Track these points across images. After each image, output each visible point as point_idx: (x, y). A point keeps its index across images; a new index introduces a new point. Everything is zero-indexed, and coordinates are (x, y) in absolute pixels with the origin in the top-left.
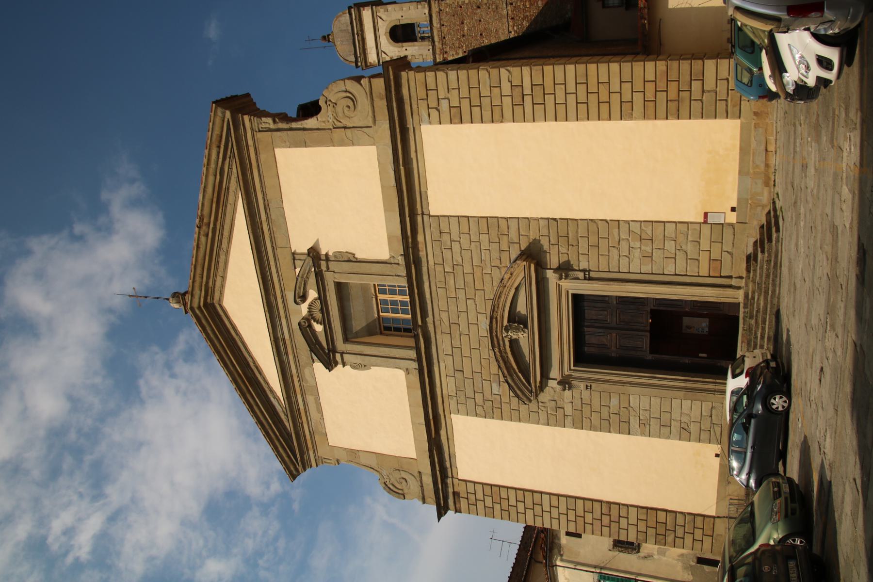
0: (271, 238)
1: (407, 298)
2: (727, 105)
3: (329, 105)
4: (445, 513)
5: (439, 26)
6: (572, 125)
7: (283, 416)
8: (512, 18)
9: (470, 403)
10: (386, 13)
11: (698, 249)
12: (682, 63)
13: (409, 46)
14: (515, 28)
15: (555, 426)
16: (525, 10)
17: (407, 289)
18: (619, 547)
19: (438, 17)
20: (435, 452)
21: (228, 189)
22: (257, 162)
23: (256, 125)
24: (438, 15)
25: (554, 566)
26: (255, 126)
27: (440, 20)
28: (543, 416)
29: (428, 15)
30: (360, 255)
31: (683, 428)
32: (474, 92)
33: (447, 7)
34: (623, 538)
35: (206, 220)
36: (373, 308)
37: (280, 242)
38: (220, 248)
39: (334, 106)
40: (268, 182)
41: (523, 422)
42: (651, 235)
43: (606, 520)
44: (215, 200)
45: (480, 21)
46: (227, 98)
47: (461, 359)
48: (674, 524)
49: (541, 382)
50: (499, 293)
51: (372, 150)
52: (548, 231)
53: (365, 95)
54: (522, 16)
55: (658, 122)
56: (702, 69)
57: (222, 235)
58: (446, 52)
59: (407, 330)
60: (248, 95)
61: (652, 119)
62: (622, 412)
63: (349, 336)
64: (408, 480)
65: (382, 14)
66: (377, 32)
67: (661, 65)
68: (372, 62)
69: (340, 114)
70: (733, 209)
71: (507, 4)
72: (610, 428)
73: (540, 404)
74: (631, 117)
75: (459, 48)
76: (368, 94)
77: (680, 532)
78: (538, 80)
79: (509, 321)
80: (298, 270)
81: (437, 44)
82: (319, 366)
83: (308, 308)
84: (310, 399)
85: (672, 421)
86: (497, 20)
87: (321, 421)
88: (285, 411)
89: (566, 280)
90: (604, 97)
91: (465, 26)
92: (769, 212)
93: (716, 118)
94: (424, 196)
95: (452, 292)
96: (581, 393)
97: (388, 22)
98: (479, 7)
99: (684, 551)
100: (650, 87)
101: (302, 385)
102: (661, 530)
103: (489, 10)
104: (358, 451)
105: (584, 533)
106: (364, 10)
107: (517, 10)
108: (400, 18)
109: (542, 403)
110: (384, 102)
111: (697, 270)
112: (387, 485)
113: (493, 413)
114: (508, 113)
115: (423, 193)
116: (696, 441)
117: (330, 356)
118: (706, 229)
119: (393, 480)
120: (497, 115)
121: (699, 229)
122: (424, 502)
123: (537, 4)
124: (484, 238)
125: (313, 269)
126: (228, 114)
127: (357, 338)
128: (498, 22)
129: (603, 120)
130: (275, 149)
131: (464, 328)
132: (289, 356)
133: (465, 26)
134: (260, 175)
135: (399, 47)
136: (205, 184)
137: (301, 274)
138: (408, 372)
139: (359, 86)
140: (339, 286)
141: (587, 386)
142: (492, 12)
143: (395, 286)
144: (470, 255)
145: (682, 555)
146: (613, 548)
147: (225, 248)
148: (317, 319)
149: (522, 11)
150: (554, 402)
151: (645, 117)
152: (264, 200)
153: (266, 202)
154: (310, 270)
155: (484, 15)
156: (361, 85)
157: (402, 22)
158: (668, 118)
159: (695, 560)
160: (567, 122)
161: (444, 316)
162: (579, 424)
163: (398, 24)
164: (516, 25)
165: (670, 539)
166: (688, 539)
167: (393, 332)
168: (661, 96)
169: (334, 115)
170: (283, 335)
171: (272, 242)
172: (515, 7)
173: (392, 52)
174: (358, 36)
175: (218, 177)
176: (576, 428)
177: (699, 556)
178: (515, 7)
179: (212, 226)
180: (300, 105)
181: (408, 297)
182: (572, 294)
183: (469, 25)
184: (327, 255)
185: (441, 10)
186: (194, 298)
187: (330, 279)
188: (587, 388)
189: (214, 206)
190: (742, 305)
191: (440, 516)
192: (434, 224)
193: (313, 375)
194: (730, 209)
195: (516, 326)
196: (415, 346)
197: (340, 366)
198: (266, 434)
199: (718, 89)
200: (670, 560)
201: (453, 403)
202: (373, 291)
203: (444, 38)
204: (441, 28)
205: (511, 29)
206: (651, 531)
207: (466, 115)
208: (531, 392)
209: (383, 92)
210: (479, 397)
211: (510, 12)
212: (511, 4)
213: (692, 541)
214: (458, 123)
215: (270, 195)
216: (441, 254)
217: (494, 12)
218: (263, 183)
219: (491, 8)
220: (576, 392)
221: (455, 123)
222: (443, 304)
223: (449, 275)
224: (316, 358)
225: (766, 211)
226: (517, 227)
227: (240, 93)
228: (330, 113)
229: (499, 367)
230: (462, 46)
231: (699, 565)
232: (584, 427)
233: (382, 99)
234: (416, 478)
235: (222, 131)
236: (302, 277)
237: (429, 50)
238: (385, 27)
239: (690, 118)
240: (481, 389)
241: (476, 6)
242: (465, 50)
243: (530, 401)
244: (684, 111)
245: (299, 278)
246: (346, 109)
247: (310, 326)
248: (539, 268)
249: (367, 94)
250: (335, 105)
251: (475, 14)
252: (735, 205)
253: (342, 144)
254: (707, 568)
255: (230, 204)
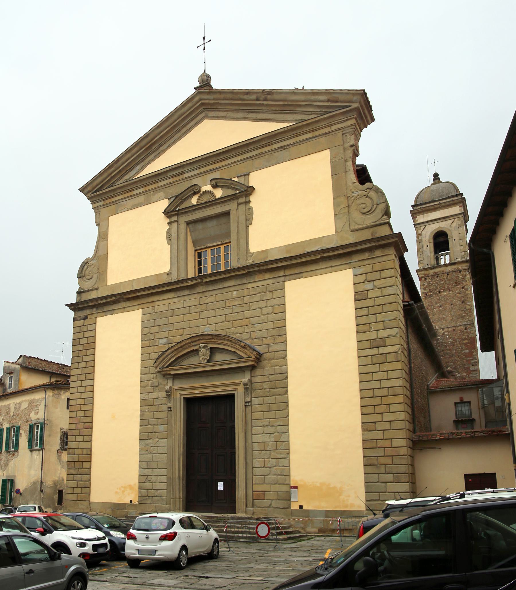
0: (259, 154)
1: (223, 269)
2: (375, 500)
3: (366, 191)
4: (71, 309)
5: (447, 271)
6: (357, 386)
7: (126, 178)
8: (454, 330)
9: (151, 323)
10: (457, 226)
11: (271, 483)
12: (406, 466)
13: (430, 248)
14: (446, 333)
15: (141, 387)
16: (461, 340)
17: (230, 268)
18: (64, 436)
19: (454, 270)
20: (113, 299)
21: (295, 113)
22: (318, 136)
23: (348, 131)
24: (456, 270)
25: (45, 390)
26: (347, 130)
27: (452, 272)
28: (146, 377)
29: (456, 261)
30: (251, 228)
31: (147, 477)
32: (379, 309)
33: (462, 277)
34: (70, 438)
35: (269, 97)
36: (213, 242)
37: (257, 162)
38: (248, 112)
39: (365, 195)
40: (302, 147)
41: (141, 363)
42: (279, 449)
43: (80, 426)
44: (286, 103)
45: (452, 305)
46: (369, 102)
47: (182, 313)
48: (82, 474)
49: (170, 375)
50: (230, 339)
51: (331, 231)
52: (278, 373)
53: (375, 221)
54: (456, 338)
55: (361, 450)
56: (402, 481)
57: (259, 113)
58: (426, 279)
59: (200, 271)
60: (373, 120)
61: (363, 446)
62: (155, 434)
63: (191, 226)
64: (92, 280)
65: (457, 223)
66: (441, 220)
67: (404, 451)
68: (417, 219)
69: (358, 202)
70: (301, 507)
71: (465, 325)
72: (143, 426)
73: (155, 375)
74: (364, 430)
75: (430, 290)
76: (375, 223)
77: (78, 478)
78: (390, 358)
79: (211, 348)
80: (236, 179)
81: (432, 271)
82: (165, 204)
83: (208, 191)
84: (141, 198)
85: (152, 469)
86: (453, 318)
87: (126, 209)
88: (130, 179)
89: (243, 389)
90: (378, 409)
91: (447, 293)
92: (300, 532)
93: (366, 492)
94: (299, 275)
95: (229, 303)
96: (166, 404)
97: (450, 228)
98: (463, 302)
99: (65, 481)
100: (387, 443)
101: (151, 191)
102: (77, 465)
103: (460, 311)
104: (108, 240)
105: (70, 411)
106: (460, 207)
107: (461, 333)
108: (454, 239)
109: (156, 376)
110: (370, 237)
111: (257, 482)
112: (86, 264)
113: (146, 341)
114: (364, 336)
115: (301, 275)
116: (139, 486)
117: (175, 212)
118: (284, 488)
119: (90, 268)
120: (361, 328)
121: (286, 483)
122: (77, 293)
123: (466, 349)
124: (271, 325)
125: (238, 192)
126: (355, 105)
127: (190, 232)
128: (451, 319)
129: (361, 409)
130: (329, 150)
131: (205, 314)
132: (171, 179)
133: (447, 293)
134: (307, 139)
135: (429, 240)
136: (298, 92)
137: (233, 182)
138: (169, 274)
139: (381, 216)
140: (227, 214)
141: (171, 408)
142: (459, 313)
143: (230, 259)
144: (258, 316)
145: (63, 480)
146: (63, 432)
147: (249, 117)
148: (202, 197)
149: (460, 337)
150: (157, 385)
151: (364, 441)
152: (288, 145)
153: (287, 147)
154: (237, 189)
155: (457, 307)
156: (383, 216)
157: (449, 240)
158: (365, 458)
159: (61, 489)
160: (359, 382)
161: (211, 299)
162: (144, 403)
163: (449, 237)
164: (449, 333)
165: (72, 471)
166: (72, 484)
167: (197, 260)
168: (381, 452)
169: (358, 197)
170: (186, 172)
171: (257, 155)
172: (463, 332)
173: (425, 235)
174: (438, 204)
175: (304, 103)
176: (141, 402)
177: (64, 492)
178: (463, 332)
179: (265, 103)
180: (366, 166)
181: (224, 270)
182: (234, 393)
183: (448, 296)
184: (250, 202)
185: (460, 272)
186: (208, 94)
187: (231, 206)
188: (169, 408)
189: (281, 103)
190: (233, 515)
191: (69, 306)
192: (278, 286)
193: (159, 200)
194: (301, 505)
195: (208, 354)
196: (188, 278)
197: (168, 221)
198: (111, 166)
199: (387, 494)
200: (59, 472)
201: (150, 310)
202: (226, 241)
203: (437, 277)
204: (445, 273)
205: (446, 329)
206: (76, 458)
207: (361, 304)
208: (163, 368)
209: (377, 235)
210: (155, 329)
211: (459, 328)
212: (466, 329)
213: (72, 486)
214: (355, 298)
215: (293, 149)
216: (257, 293)
217: (459, 315)
218: (303, 142)
219: (462, 312)
220: (164, 401)
221: (355, 296)
222: (220, 297)
223: (241, 300)
224: (172, 200)
225: (301, 530)
226: (279, 350)
227: (374, 112)
228: (360, 192)
229: (178, 343)
230: (431, 292)
231: (58, 491)
232: (142, 407)
233: (372, 235)
234: (93, 286)
235: (341, 102)
236: (232, 184)
237: (427, 265)
238: (445, 226)
239: (365, 474)
240: (162, 330)
241: (463, 300)
242: (428, 294)
243: (156, 368)
244: (370, 469)
245: (230, 182)
246: (364, 206)
247: (195, 193)
248: (251, 368)
249: (376, 222)
250: (366, 196)
251: (457, 300)
252: (304, 508)
253: (336, 205)
254: (56, 497)
255: (283, 117)
